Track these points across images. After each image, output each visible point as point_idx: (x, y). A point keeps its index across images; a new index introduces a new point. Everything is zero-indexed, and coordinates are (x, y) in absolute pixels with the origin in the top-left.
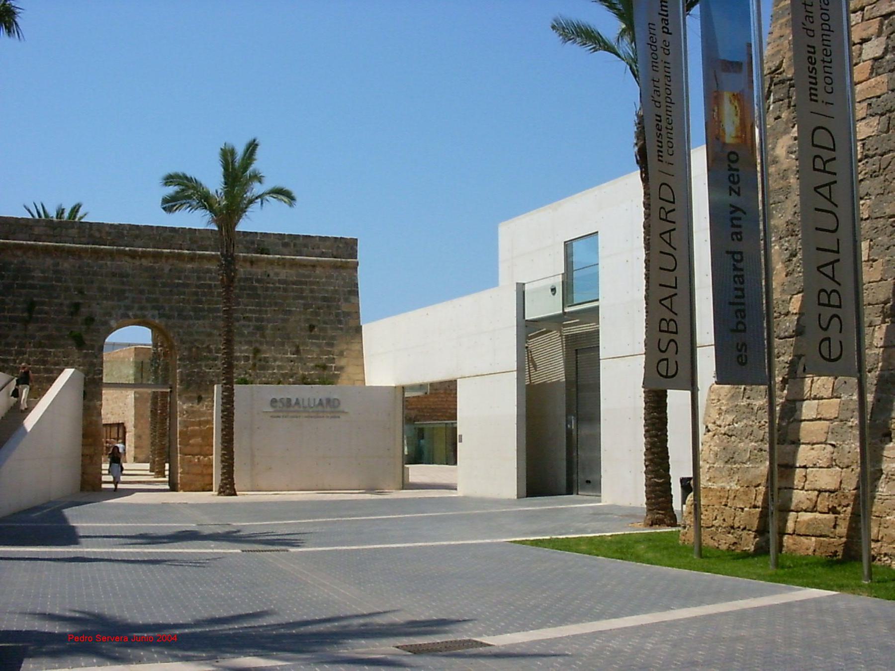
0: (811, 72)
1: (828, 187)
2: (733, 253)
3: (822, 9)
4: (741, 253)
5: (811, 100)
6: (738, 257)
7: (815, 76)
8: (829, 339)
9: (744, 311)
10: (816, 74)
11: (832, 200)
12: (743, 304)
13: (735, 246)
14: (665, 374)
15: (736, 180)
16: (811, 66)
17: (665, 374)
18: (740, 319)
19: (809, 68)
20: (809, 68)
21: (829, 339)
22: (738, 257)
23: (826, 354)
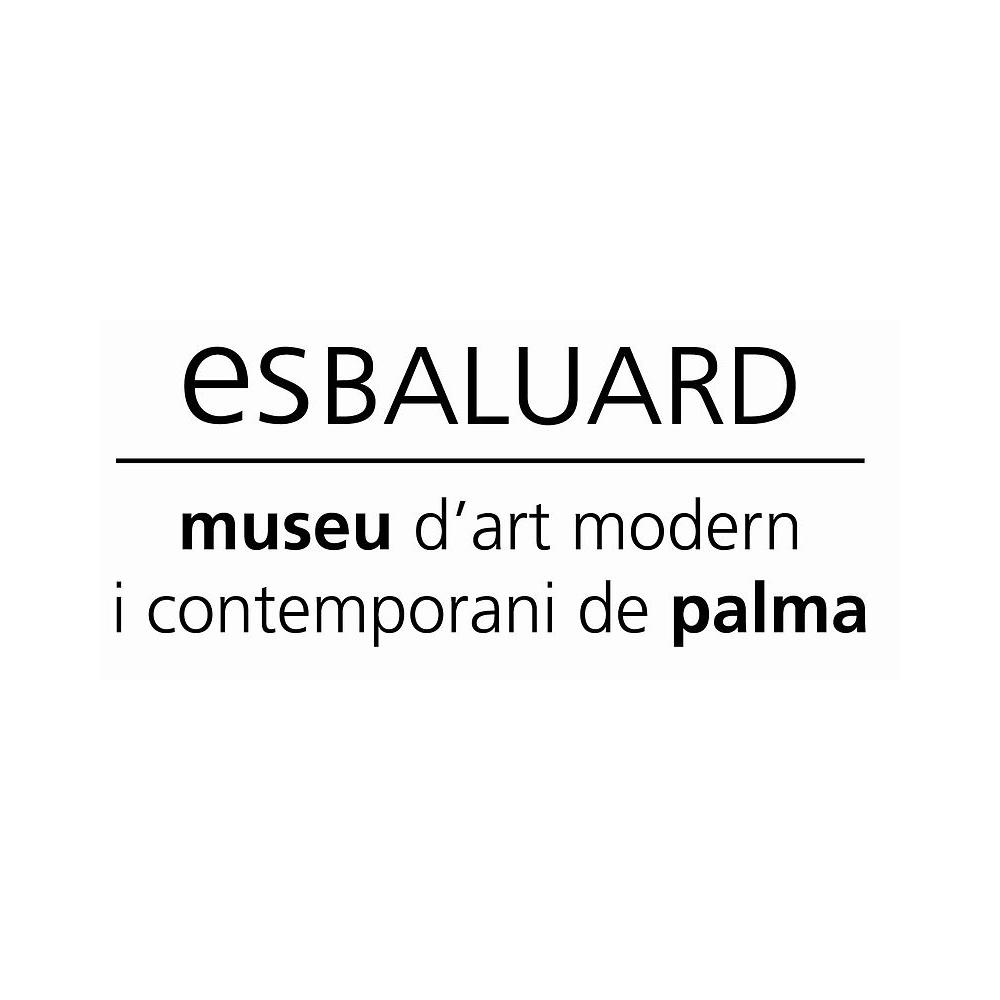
0: (290, 523)
1: (637, 393)
2: (680, 626)
3: (455, 604)
4: (680, 604)
5: (188, 521)
6: (691, 614)
7: (281, 543)
8: (242, 381)
9: (741, 626)
10: (289, 546)
11: (607, 407)
12: (760, 627)
13: (661, 619)
14: (200, 376)
15: (331, 538)
16: (310, 526)
17: (198, 377)
18: (713, 613)
19: (304, 517)
20: (304, 517)
21: (242, 381)
22: (691, 614)
23: (207, 370)
